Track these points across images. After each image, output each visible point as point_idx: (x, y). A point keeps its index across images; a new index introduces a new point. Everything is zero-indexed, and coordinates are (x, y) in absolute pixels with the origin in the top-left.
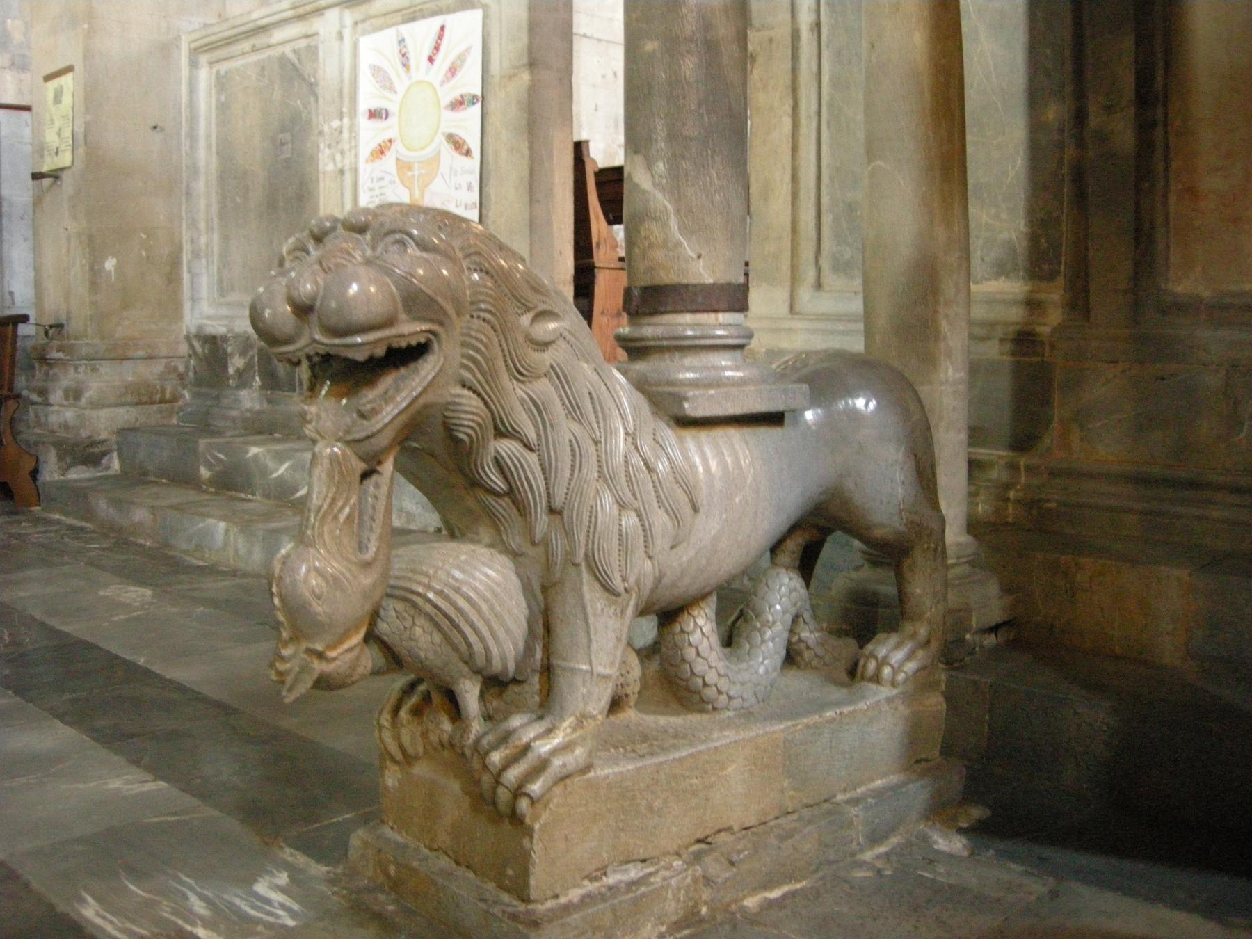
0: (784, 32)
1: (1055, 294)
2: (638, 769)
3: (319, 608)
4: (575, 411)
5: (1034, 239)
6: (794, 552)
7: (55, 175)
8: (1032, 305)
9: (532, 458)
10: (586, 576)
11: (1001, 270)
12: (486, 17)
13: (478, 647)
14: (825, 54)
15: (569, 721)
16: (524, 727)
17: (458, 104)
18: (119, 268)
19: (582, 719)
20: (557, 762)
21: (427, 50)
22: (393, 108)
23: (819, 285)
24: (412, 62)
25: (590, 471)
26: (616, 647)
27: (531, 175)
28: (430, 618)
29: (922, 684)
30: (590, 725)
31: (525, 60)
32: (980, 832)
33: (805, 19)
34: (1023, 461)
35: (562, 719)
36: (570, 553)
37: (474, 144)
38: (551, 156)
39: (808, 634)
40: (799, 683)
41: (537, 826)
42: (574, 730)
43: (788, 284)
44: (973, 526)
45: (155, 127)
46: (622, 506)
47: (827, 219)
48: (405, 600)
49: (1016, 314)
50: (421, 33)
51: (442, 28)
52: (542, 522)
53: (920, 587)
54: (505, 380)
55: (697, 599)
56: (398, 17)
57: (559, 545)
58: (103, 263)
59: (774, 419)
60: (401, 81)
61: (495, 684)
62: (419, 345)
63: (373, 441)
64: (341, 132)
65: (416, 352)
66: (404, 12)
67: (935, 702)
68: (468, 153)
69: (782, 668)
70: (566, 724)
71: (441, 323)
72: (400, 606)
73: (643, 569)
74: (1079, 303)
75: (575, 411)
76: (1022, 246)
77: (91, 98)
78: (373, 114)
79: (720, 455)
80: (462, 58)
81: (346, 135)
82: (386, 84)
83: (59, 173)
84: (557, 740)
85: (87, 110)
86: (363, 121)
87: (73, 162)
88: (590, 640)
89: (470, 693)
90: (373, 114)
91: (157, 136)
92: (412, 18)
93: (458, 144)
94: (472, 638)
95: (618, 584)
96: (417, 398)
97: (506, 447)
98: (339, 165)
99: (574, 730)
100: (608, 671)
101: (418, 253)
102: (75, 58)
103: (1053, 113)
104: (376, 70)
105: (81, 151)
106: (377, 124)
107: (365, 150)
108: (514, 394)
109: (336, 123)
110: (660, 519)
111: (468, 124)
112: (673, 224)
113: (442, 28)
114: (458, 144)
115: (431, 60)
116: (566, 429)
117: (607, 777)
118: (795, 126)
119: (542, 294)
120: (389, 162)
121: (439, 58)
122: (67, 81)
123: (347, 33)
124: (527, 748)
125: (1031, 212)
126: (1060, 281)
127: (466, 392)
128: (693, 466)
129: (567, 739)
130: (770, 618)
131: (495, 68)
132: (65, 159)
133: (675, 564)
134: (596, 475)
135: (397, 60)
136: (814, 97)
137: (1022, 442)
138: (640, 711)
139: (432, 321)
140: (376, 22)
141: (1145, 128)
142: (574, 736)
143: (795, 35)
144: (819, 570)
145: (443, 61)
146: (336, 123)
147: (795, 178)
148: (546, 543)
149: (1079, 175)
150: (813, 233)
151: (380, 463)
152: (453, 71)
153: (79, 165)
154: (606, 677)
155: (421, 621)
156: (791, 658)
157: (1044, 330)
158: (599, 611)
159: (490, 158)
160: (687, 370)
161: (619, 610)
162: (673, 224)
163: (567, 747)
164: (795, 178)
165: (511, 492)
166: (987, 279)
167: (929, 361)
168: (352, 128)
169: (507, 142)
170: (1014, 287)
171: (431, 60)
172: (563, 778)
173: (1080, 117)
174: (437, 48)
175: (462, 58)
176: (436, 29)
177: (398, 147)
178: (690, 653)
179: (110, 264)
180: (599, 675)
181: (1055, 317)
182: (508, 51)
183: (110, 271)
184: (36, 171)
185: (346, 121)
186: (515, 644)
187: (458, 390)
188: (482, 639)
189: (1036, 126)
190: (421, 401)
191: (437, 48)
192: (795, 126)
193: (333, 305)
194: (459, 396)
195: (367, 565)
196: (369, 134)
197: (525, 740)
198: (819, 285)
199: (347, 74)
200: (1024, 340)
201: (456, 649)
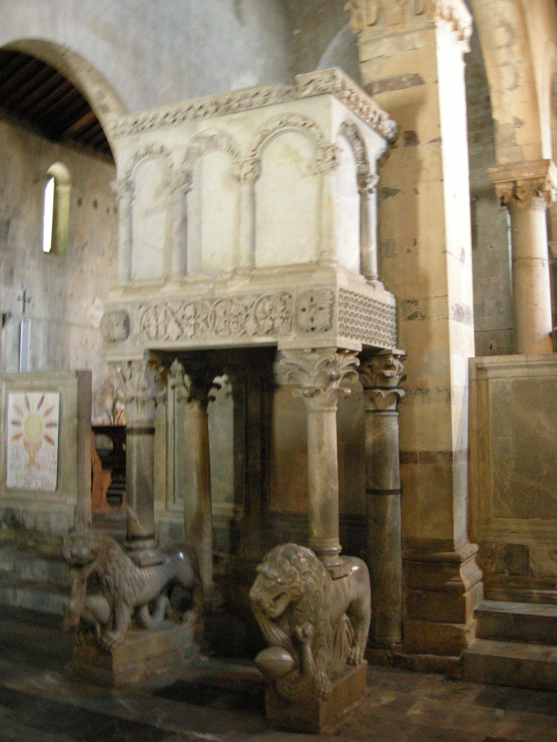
0: (164, 423)
1: (241, 509)
4: (120, 567)
5: (235, 494)
8: (235, 511)
11: (227, 500)
14: (176, 430)
16: (110, 634)
17: (50, 425)
23: (174, 501)
24: (31, 408)
25: (123, 579)
27: (78, 455)
29: (197, 621)
32: (212, 657)
33: (170, 419)
34: (233, 558)
36: (119, 597)
39: (170, 611)
40: (167, 623)
43: (165, 501)
44: (216, 578)
47: (176, 481)
49: (231, 514)
50: (35, 397)
51: (43, 398)
53: (197, 599)
55: (144, 604)
57: (117, 595)
59: (161, 563)
60: (26, 413)
61: (104, 626)
67: (202, 626)
69: (171, 152)
73: (134, 599)
74: (247, 512)
75: (120, 567)
76: (232, 494)
79: (148, 572)
89: (98, 628)
93: (49, 440)
103: (240, 457)
108: (109, 567)
110: (137, 589)
111: (54, 433)
112: (138, 523)
113: (43, 398)
114: (49, 440)
116: (118, 570)
118: (167, 452)
120: (21, 441)
125: (235, 485)
126: (243, 505)
128: (142, 575)
135: (25, 406)
136: (173, 441)
137: (233, 550)
141: (263, 465)
143: (167, 424)
144: (172, 596)
145: (43, 408)
147: (167, 468)
148: (114, 596)
149: (247, 476)
150: (172, 486)
156: (166, 617)
157: (238, 520)
159: (62, 446)
160: (141, 555)
162: (138, 523)
164: (167, 468)
167: (201, 538)
170: (230, 506)
173: (247, 460)
178: (143, 617)
181: (241, 515)
182: (70, 411)
192: (167, 452)
196: (12, 430)
198: (174, 501)
200: (232, 523)
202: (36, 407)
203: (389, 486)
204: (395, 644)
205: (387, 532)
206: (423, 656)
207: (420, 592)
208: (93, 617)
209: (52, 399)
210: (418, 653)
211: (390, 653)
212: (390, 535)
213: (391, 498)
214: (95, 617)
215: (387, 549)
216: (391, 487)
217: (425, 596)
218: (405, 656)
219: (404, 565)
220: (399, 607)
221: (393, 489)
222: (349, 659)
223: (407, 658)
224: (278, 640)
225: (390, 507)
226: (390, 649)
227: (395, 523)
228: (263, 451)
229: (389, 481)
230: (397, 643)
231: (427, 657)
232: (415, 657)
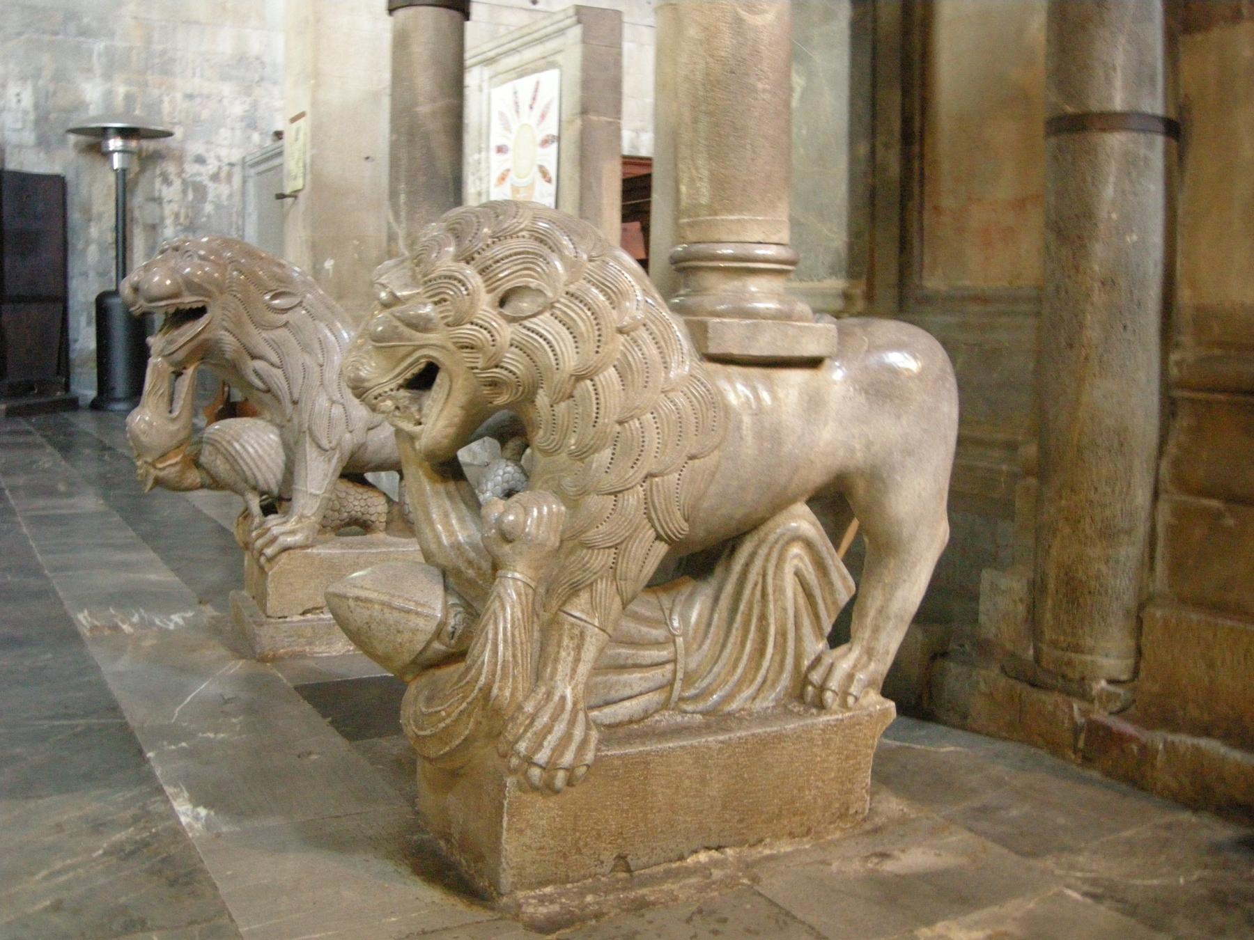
2: (343, 554)
3: (143, 438)
4: (306, 348)
6: (514, 450)
7: (294, 195)
9: (278, 372)
10: (308, 438)
11: (833, 271)
12: (561, 75)
13: (248, 473)
15: (294, 518)
17: (545, 143)
18: (336, 266)
19: (302, 517)
20: (281, 539)
21: (528, 102)
22: (510, 144)
26: (323, 480)
28: (224, 455)
30: (306, 522)
31: (578, 110)
35: (292, 517)
37: (553, 173)
38: (599, 179)
41: (270, 573)
42: (297, 523)
45: (367, 158)
46: (333, 402)
48: (213, 445)
51: (538, 83)
52: (289, 408)
54: (251, 328)
56: (513, 74)
58: (323, 263)
62: (198, 309)
63: (175, 355)
64: (479, 163)
65: (198, 313)
66: (517, 70)
68: (549, 181)
70: (292, 520)
71: (210, 297)
72: (211, 448)
77: (317, 136)
78: (501, 150)
80: (547, 107)
81: (483, 165)
82: (507, 127)
83: (296, 194)
84: (288, 527)
85: (313, 146)
86: (493, 154)
87: (304, 185)
88: (307, 474)
90: (501, 150)
91: (369, 164)
92: (521, 76)
93: (544, 173)
94: (245, 468)
95: (325, 443)
96: (199, 333)
97: (259, 364)
98: (478, 189)
99: (297, 523)
100: (318, 492)
101: (199, 262)
102: (305, 107)
104: (502, 114)
105: (309, 177)
106: (501, 157)
107: (494, 178)
109: (476, 156)
111: (549, 157)
113: (538, 83)
115: (531, 107)
117: (319, 554)
119: (285, 282)
121: (535, 106)
122: (301, 122)
123: (485, 85)
124: (269, 529)
125: (850, 226)
127: (226, 333)
129: (292, 528)
130: (485, 488)
131: (564, 117)
132: (299, 184)
133: (375, 439)
134: (318, 383)
138: (388, 534)
139: (202, 295)
140: (502, 77)
141: (906, 159)
142: (297, 527)
146: (476, 156)
151: (185, 368)
152: (543, 116)
153: (308, 188)
154: (317, 496)
155: (220, 457)
158: (314, 458)
161: (327, 459)
163: (293, 532)
165: (268, 391)
166: (825, 278)
168: (488, 158)
169: (569, 171)
171: (531, 107)
172: (286, 549)
173: (873, 152)
174: (534, 99)
175: (547, 107)
176: (534, 84)
177: (512, 175)
179: (329, 264)
180: (311, 494)
183: (328, 270)
184: (279, 192)
185: (483, 154)
186: (275, 475)
187: (223, 332)
188: (251, 469)
189: (853, 161)
190: (202, 337)
191: (534, 99)
193: (146, 287)
194: (224, 335)
195: (174, 420)
197: (269, 526)
199: (485, 119)
201: (238, 474)
202: (527, 108)
203: (1110, 99)
204: (1103, 683)
205: (1096, 268)
206: (1184, 741)
207: (1215, 504)
208: (228, 467)
209: (550, 81)
210: (1176, 729)
211: (1084, 713)
212: (1108, 283)
213: (1115, 142)
214: (233, 468)
215: (1093, 333)
216: (1118, 103)
217: (1230, 522)
218: (1128, 728)
219: (1169, 408)
220: (1130, 552)
221: (1126, 109)
222: (802, 680)
223: (1131, 739)
224: (439, 542)
225: (1112, 179)
226: (1085, 696)
227: (1132, 238)
228: (907, 121)
229: (1108, 79)
230: (1111, 682)
231: (1197, 749)
232: (1158, 739)
